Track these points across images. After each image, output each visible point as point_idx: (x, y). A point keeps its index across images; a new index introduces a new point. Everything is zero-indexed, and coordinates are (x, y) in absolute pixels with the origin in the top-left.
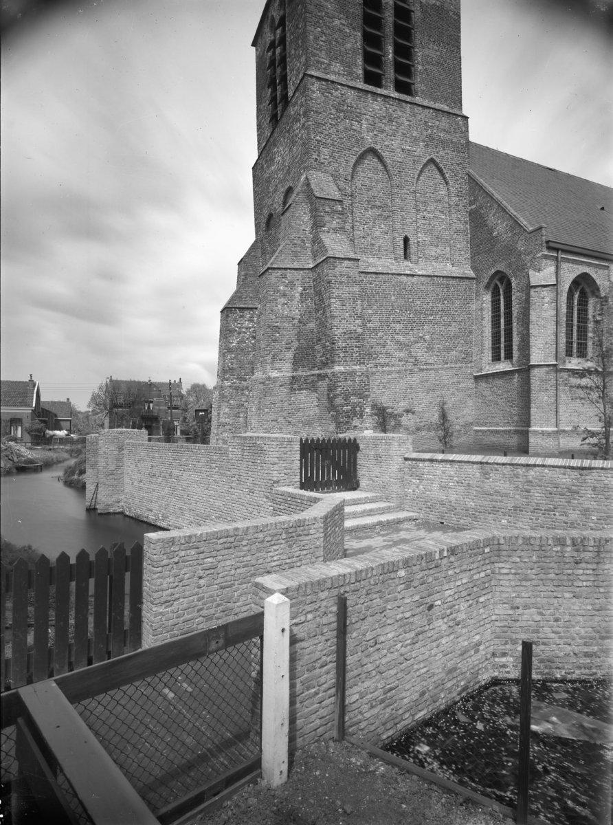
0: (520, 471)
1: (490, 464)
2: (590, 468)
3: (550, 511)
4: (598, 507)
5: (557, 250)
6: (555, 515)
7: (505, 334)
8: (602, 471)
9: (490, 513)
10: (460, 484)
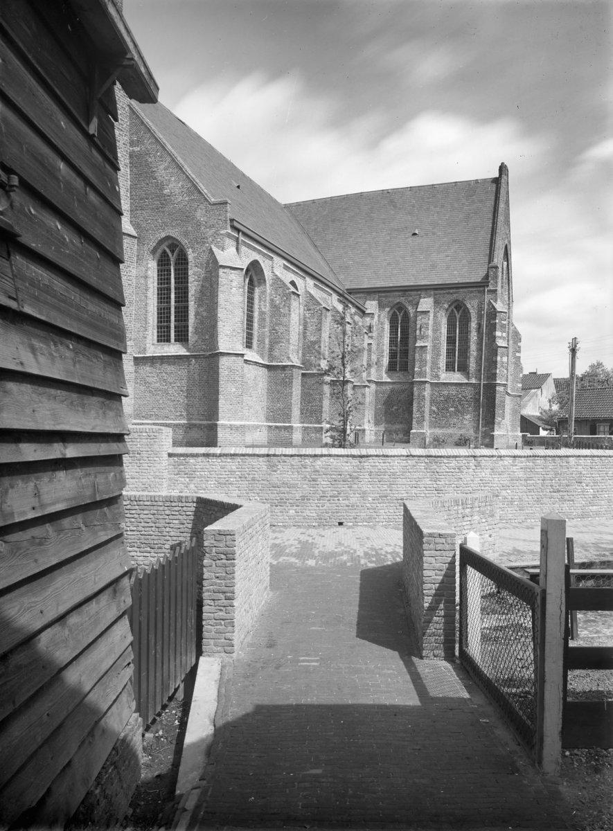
0: (308, 461)
1: (277, 456)
2: (367, 456)
3: (335, 497)
4: (373, 489)
5: (238, 231)
6: (339, 500)
7: (175, 312)
8: (377, 458)
9: (277, 506)
10: (243, 479)
